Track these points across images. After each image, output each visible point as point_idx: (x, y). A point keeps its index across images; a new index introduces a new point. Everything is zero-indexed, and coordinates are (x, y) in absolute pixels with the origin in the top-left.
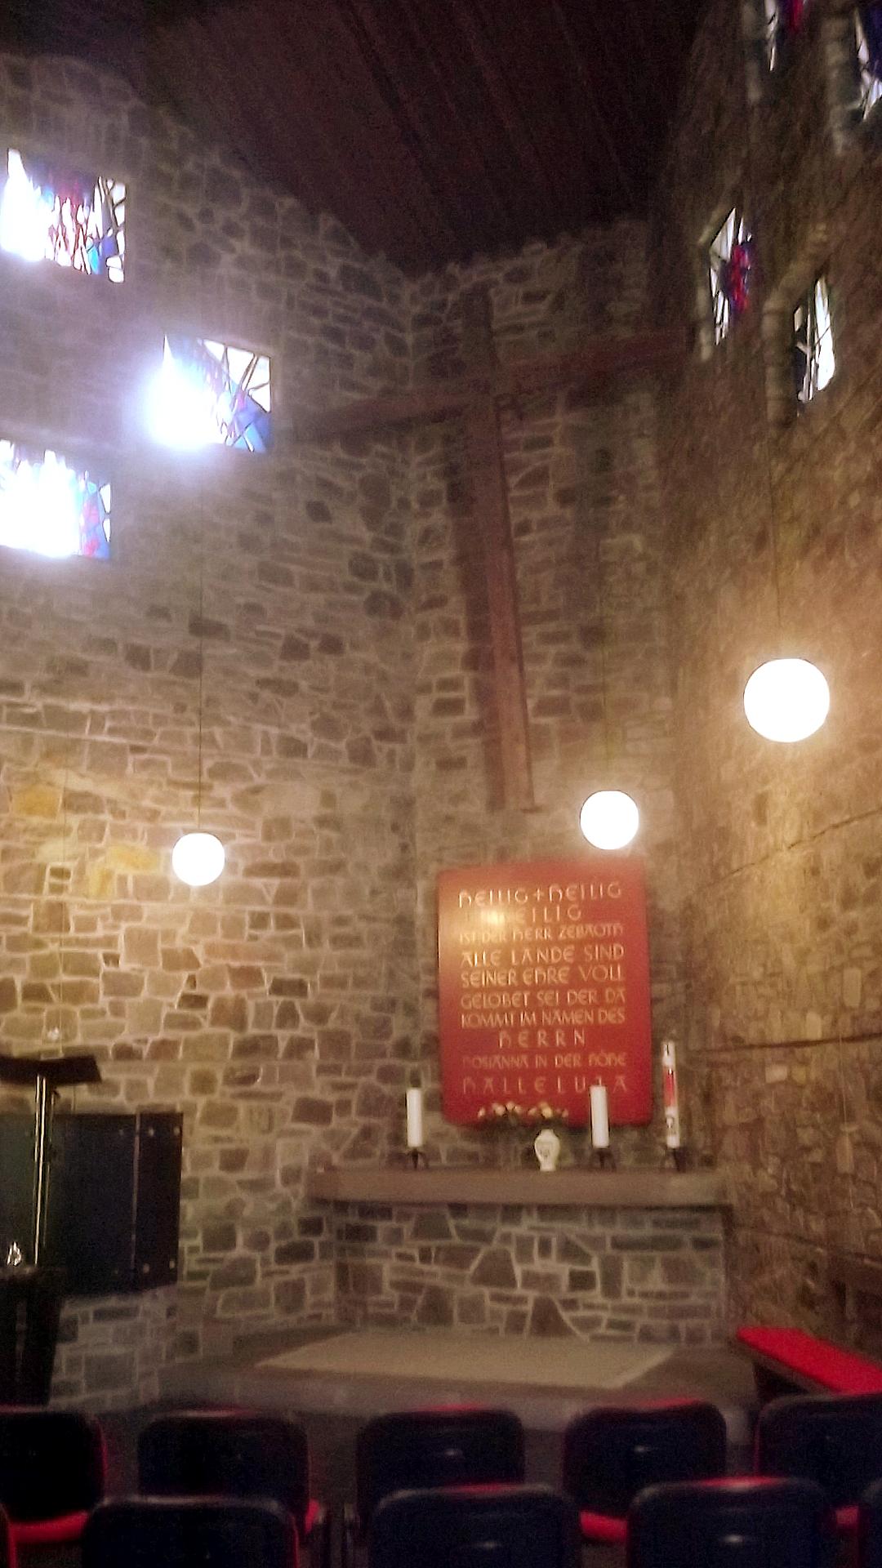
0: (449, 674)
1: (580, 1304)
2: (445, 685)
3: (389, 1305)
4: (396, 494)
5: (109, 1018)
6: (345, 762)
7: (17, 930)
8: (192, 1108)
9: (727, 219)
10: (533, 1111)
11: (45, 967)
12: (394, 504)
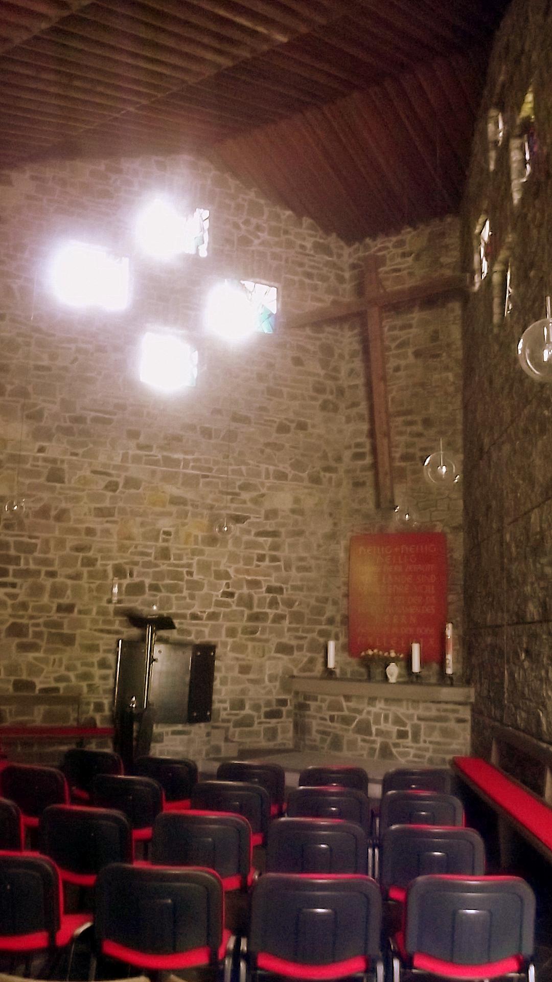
0: (359, 440)
1: (401, 745)
2: (358, 445)
3: (315, 741)
4: (337, 352)
5: (188, 600)
6: (306, 483)
7: (147, 559)
8: (225, 644)
9: (485, 224)
10: (386, 654)
11: (159, 575)
12: (336, 356)
